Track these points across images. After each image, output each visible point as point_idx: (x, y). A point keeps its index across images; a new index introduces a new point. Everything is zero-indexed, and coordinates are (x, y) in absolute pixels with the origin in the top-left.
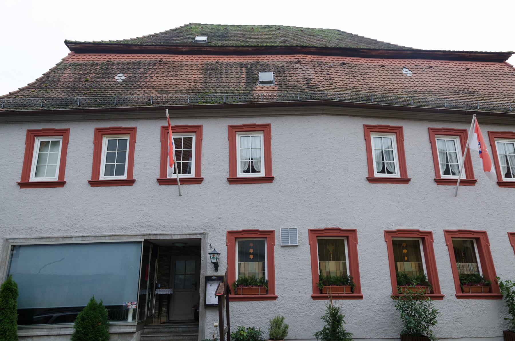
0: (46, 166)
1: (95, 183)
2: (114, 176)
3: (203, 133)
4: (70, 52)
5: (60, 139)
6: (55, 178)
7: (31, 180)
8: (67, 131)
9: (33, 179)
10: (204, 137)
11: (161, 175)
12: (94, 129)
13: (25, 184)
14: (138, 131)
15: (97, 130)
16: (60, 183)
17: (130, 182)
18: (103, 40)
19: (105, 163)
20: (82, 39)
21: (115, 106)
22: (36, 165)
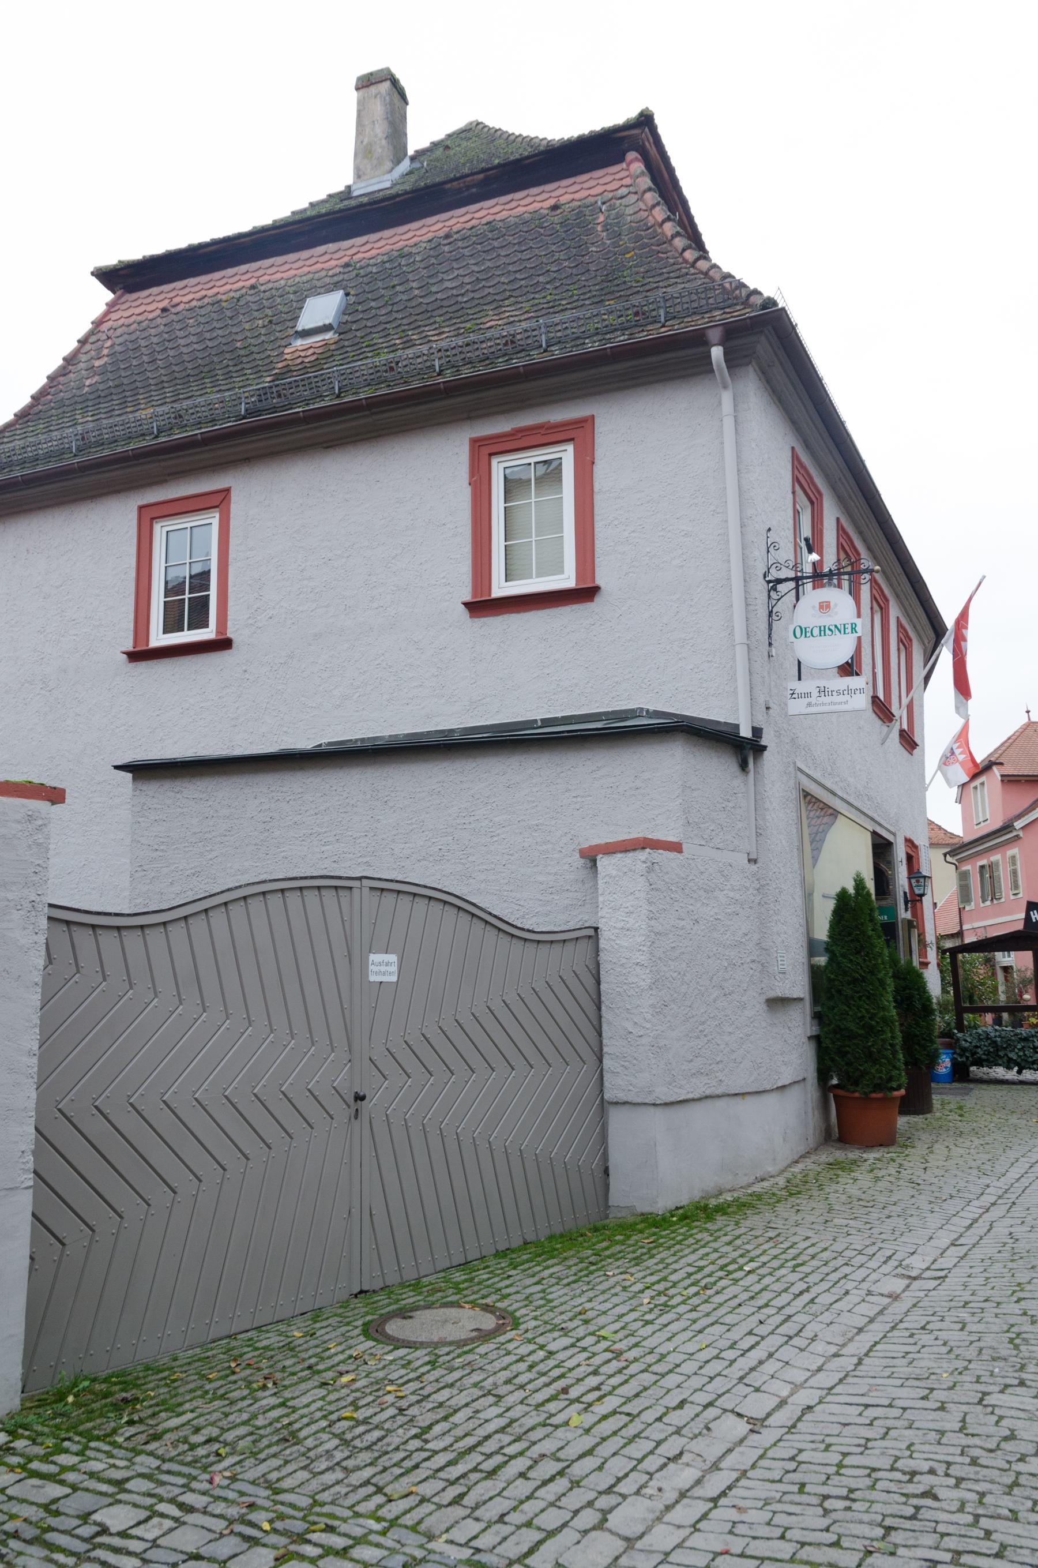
0: (532, 540)
1: (140, 655)
2: (186, 632)
3: (598, 440)
4: (109, 296)
5: (567, 455)
6: (567, 580)
7: (497, 593)
8: (586, 424)
9: (501, 588)
10: (599, 453)
11: (475, 593)
12: (136, 508)
13: (482, 606)
14: (234, 496)
15: (477, 444)
16: (585, 593)
17: (222, 644)
18: (593, 129)
19: (162, 599)
20: (135, 253)
21: (157, 437)
22: (503, 543)
